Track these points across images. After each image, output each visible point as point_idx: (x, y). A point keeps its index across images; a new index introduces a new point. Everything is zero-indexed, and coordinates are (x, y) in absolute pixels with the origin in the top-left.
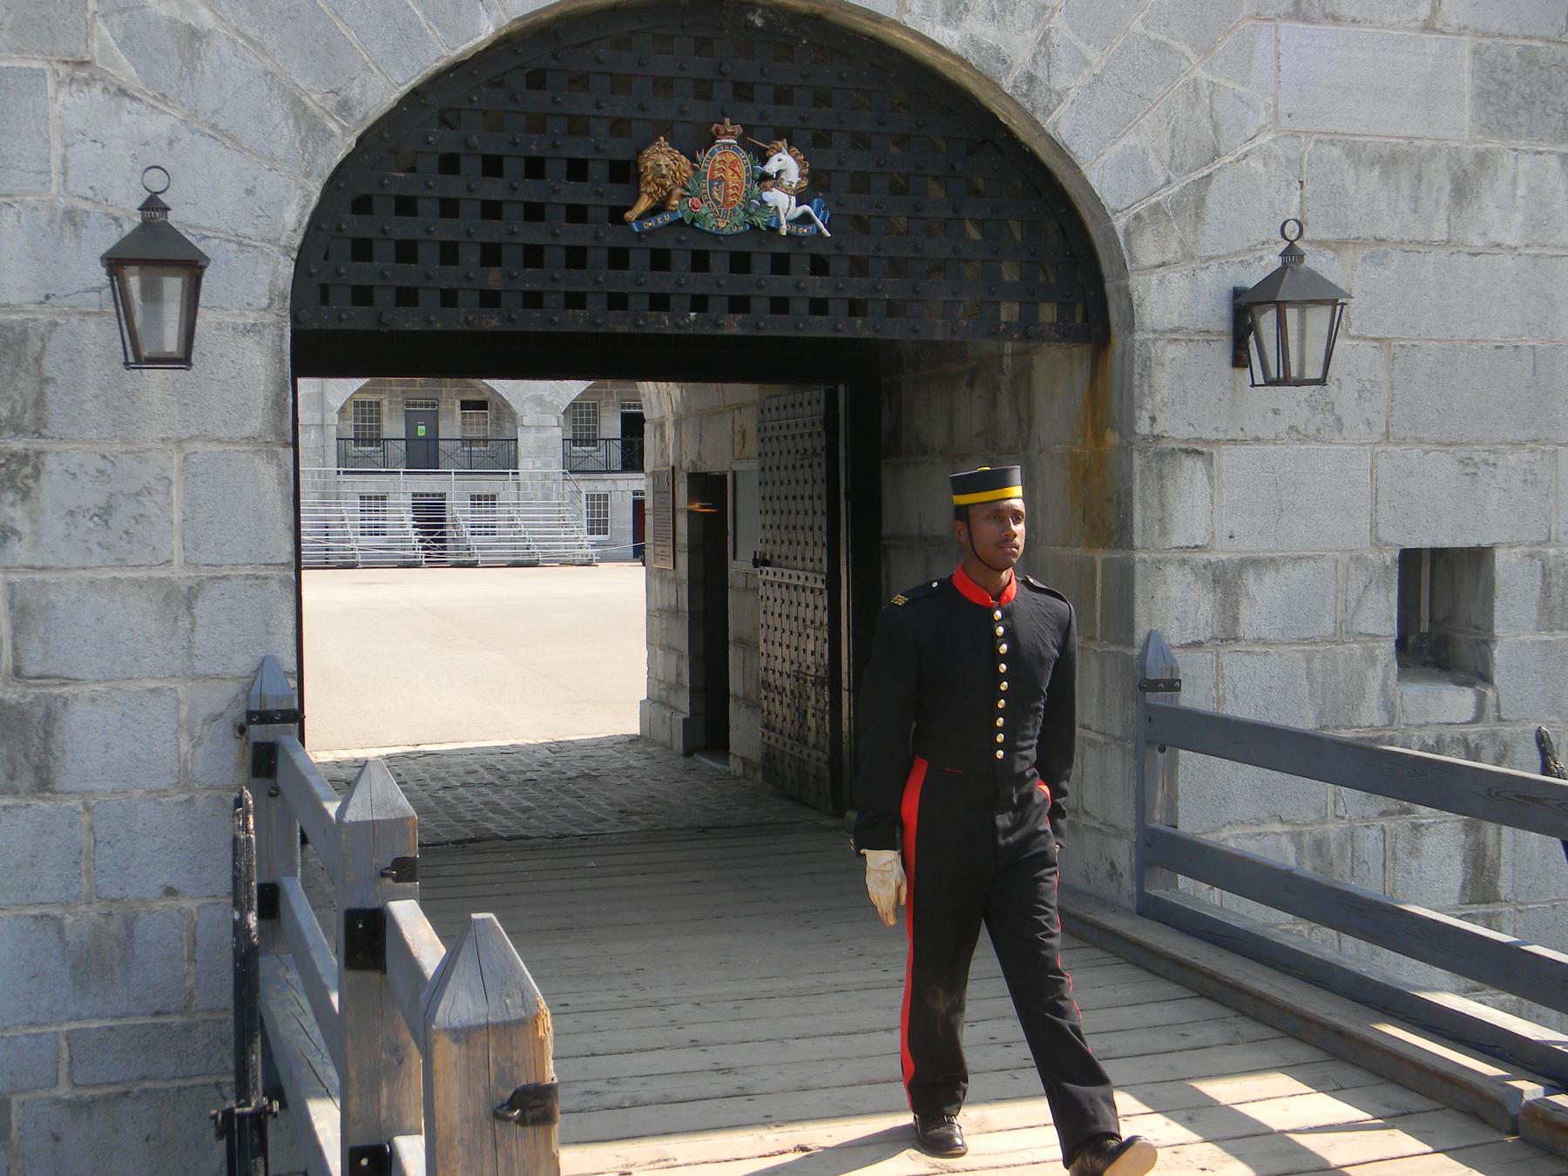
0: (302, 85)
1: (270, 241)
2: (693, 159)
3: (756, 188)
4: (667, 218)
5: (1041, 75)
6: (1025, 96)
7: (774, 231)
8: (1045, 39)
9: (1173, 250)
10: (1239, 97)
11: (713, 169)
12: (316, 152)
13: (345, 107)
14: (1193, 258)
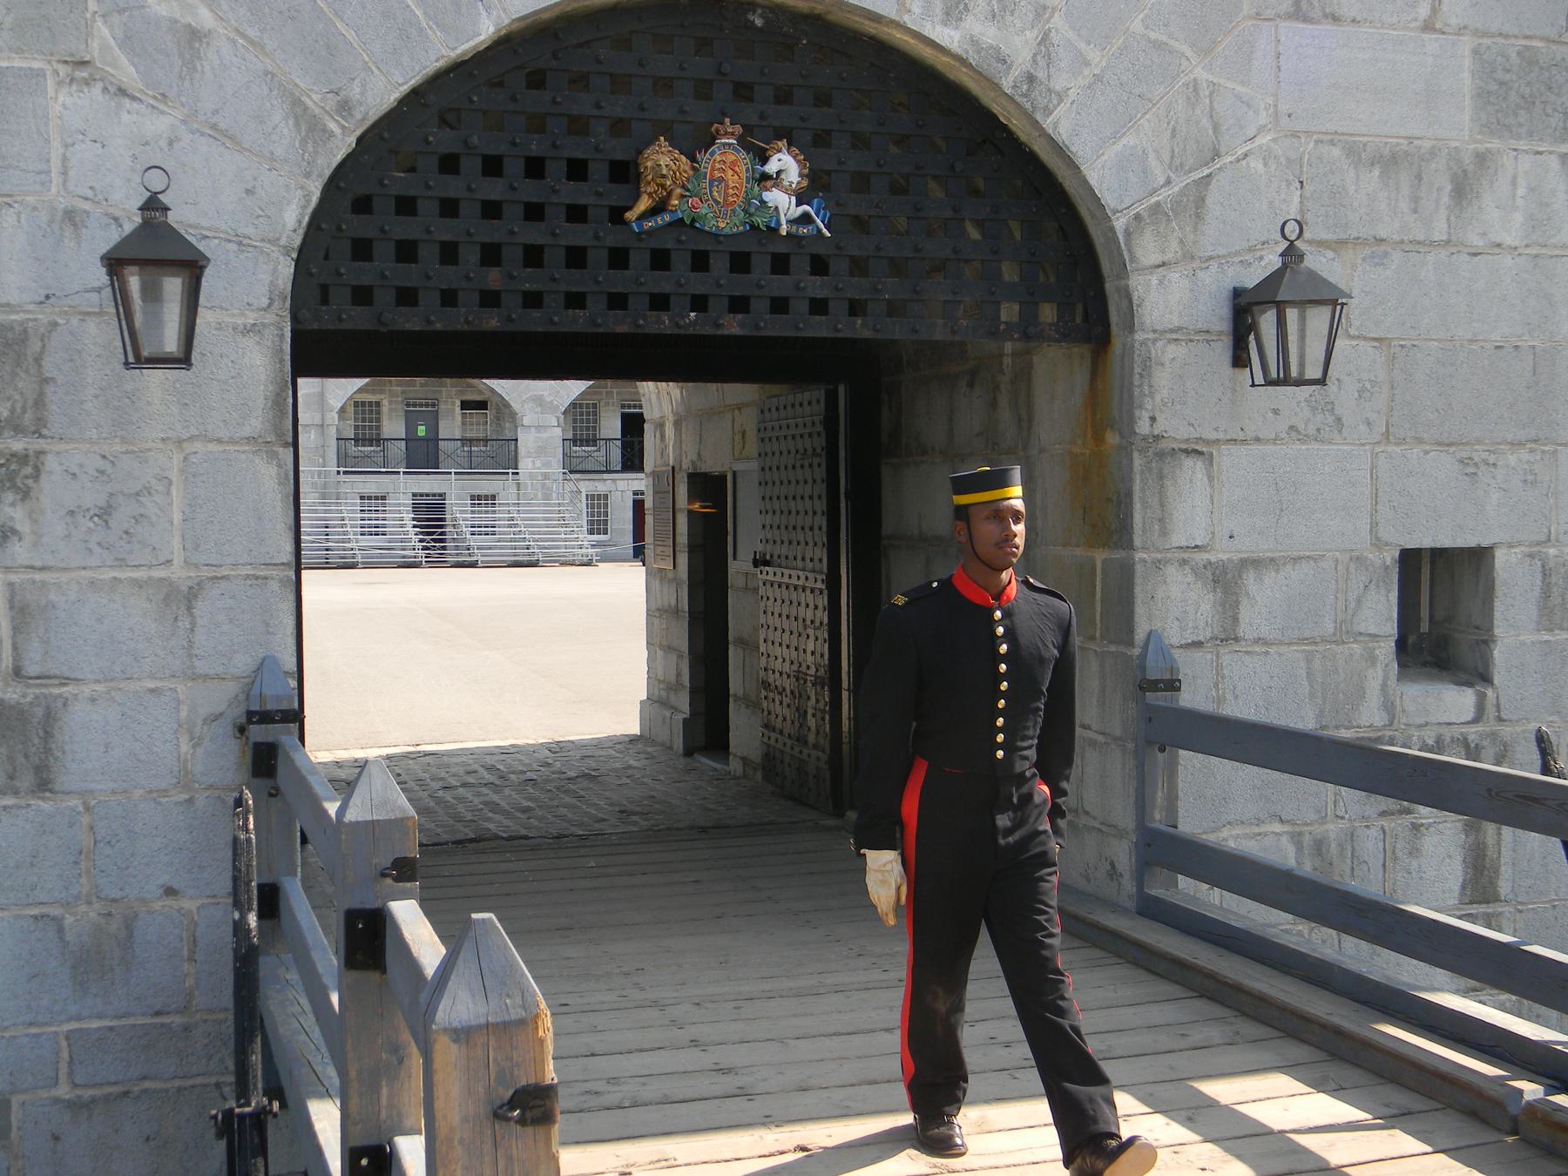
0: (302, 85)
1: (270, 241)
2: (693, 159)
3: (756, 188)
4: (667, 218)
5: (1041, 75)
6: (1025, 96)
7: (774, 231)
8: (1045, 39)
9: (1173, 250)
10: (1239, 97)
11: (713, 169)
12: (316, 152)
13: (345, 107)
14: (1193, 258)
